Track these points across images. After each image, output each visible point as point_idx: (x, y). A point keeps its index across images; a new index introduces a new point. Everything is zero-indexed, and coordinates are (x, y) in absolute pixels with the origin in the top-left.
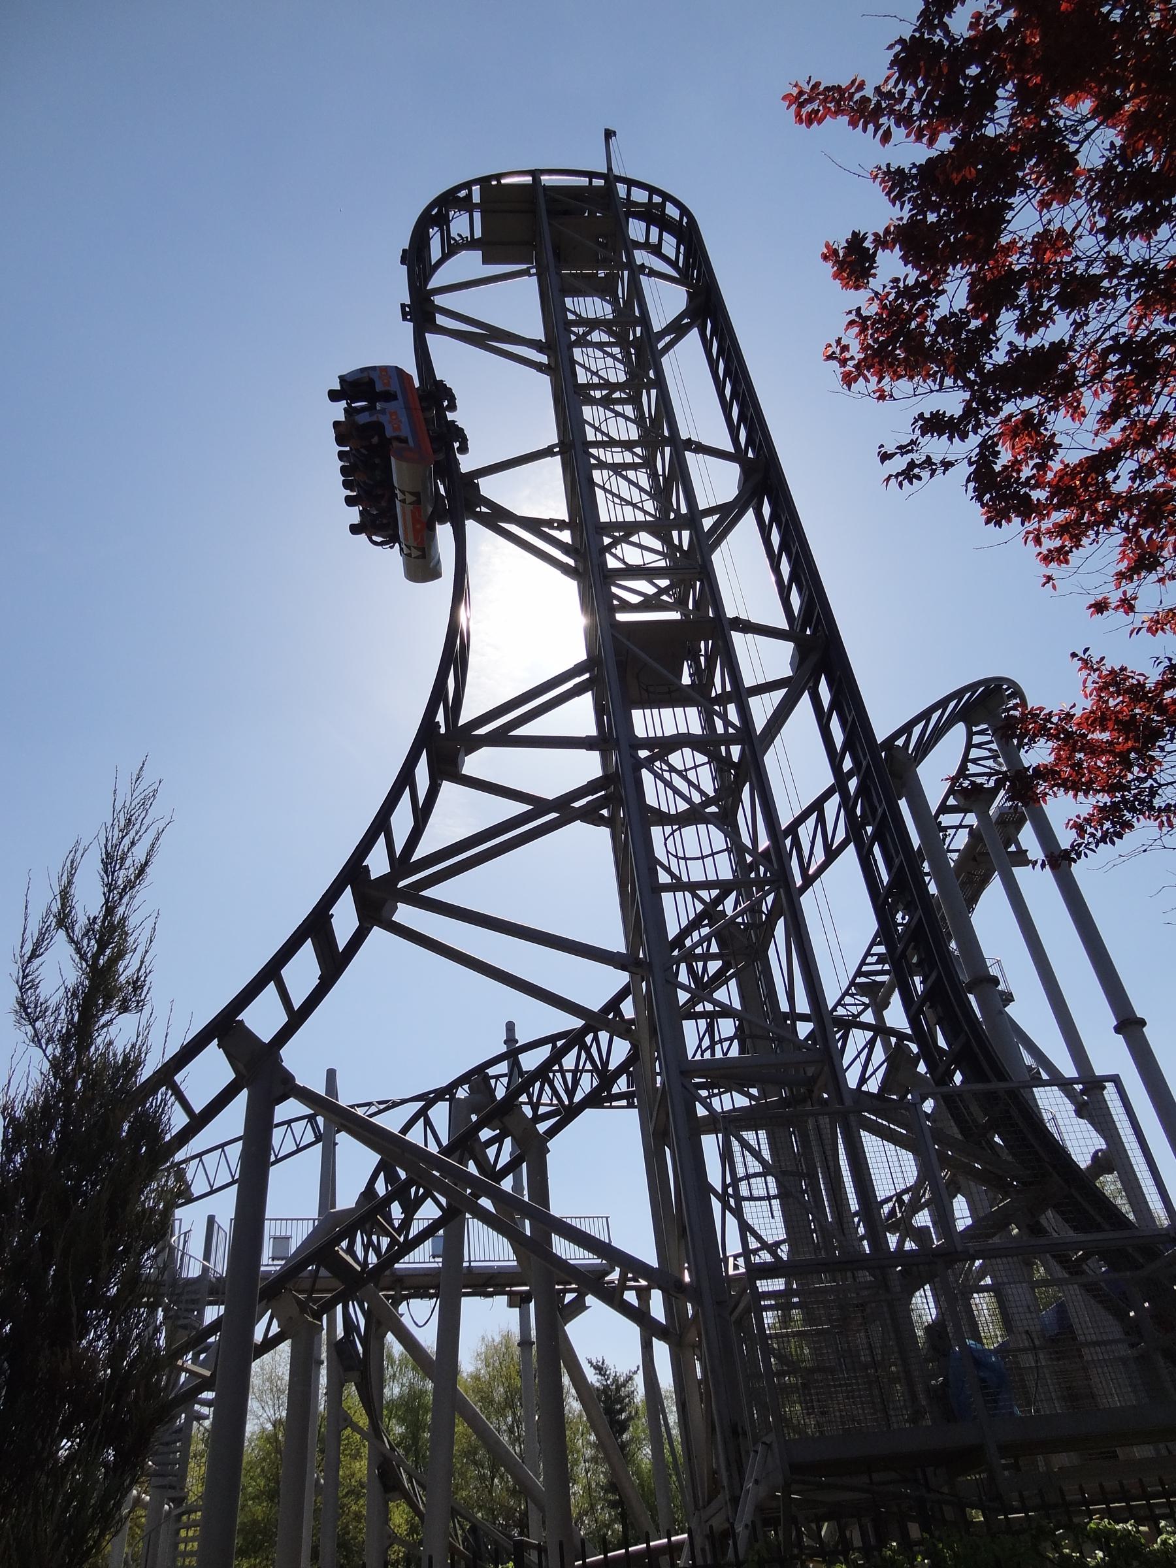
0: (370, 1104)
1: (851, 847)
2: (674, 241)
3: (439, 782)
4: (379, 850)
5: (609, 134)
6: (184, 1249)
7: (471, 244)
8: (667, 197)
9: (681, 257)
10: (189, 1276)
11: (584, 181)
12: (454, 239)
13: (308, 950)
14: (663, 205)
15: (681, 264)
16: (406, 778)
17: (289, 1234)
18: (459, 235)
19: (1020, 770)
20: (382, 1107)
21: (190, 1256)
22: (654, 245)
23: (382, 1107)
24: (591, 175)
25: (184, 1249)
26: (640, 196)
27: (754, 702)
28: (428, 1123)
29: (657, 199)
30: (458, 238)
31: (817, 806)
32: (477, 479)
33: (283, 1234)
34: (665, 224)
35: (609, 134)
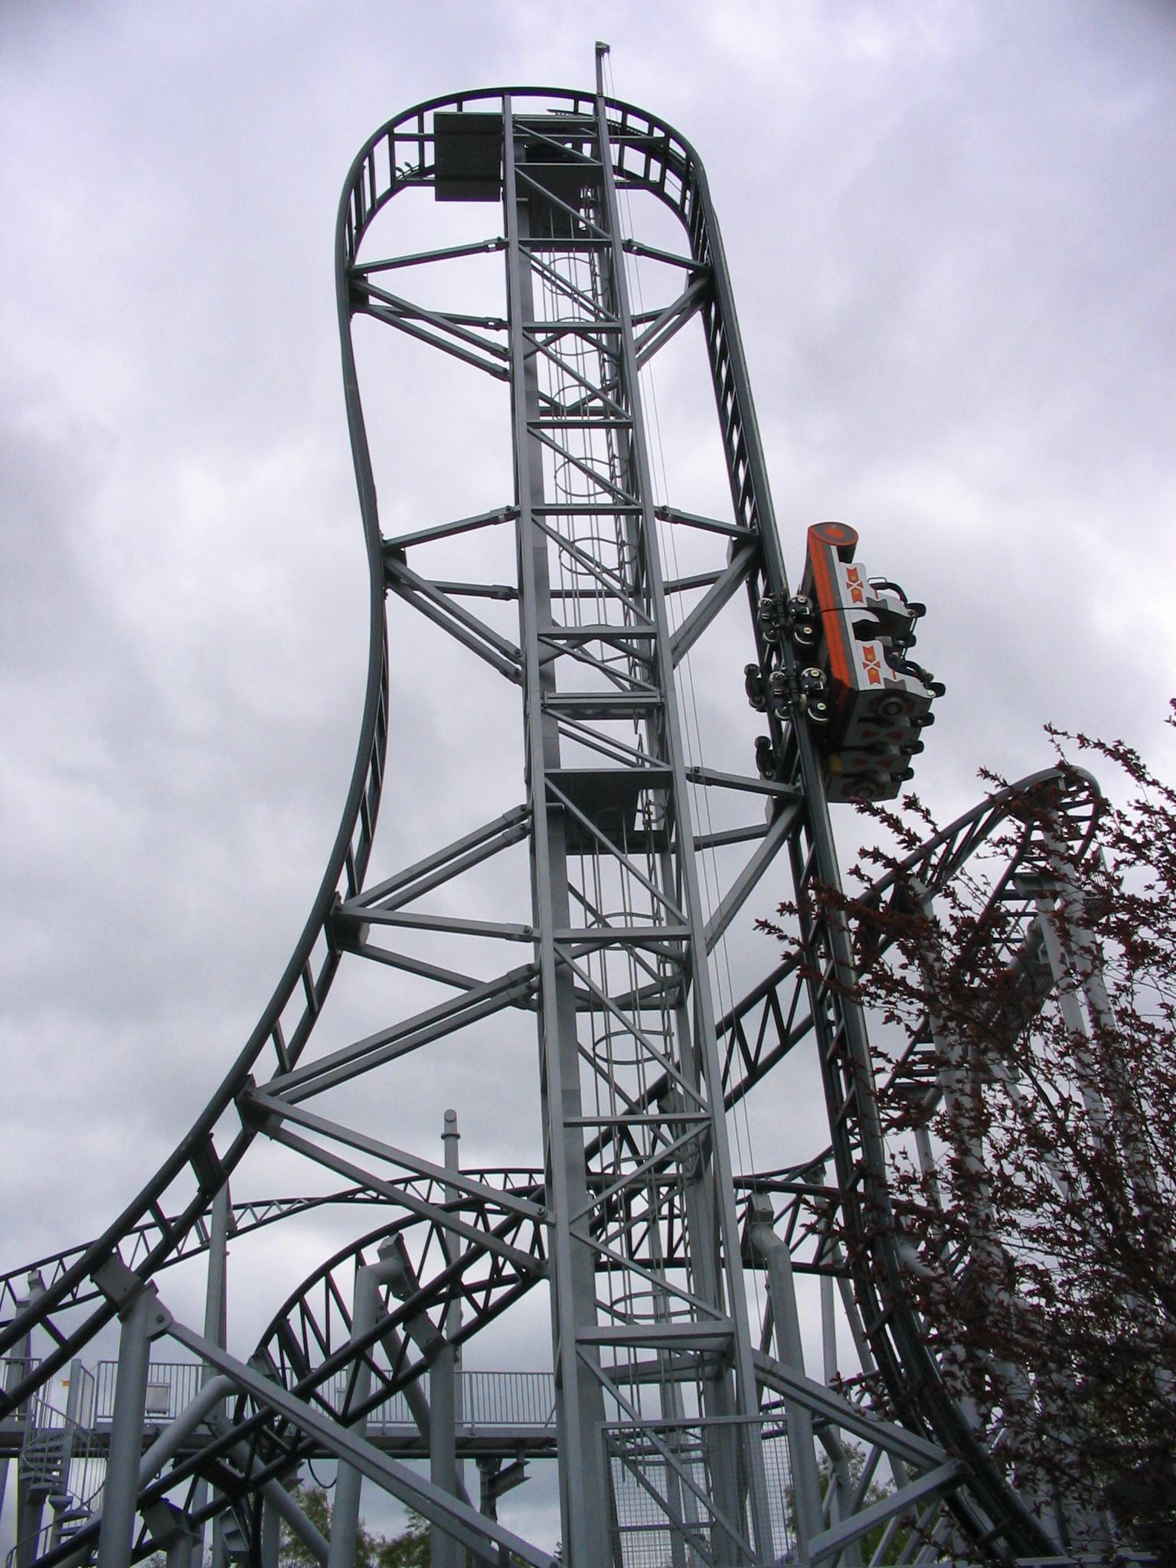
0: (268, 1203)
1: (812, 1033)
2: (679, 183)
3: (339, 952)
4: (269, 1052)
5: (601, 51)
6: (44, 1399)
7: (418, 176)
8: (670, 133)
9: (687, 203)
10: (53, 1426)
11: (567, 105)
12: (400, 170)
13: (188, 1170)
14: (665, 140)
15: (687, 211)
16: (299, 967)
17: (167, 1381)
18: (407, 164)
19: (779, 1246)
20: (285, 1207)
21: (52, 1409)
22: (655, 183)
23: (285, 1207)
24: (577, 96)
25: (44, 1399)
26: (642, 126)
27: (704, 862)
28: (330, 1285)
29: (658, 133)
30: (406, 169)
31: (767, 990)
32: (404, 547)
33: (161, 1380)
34: (669, 162)
35: (601, 51)
